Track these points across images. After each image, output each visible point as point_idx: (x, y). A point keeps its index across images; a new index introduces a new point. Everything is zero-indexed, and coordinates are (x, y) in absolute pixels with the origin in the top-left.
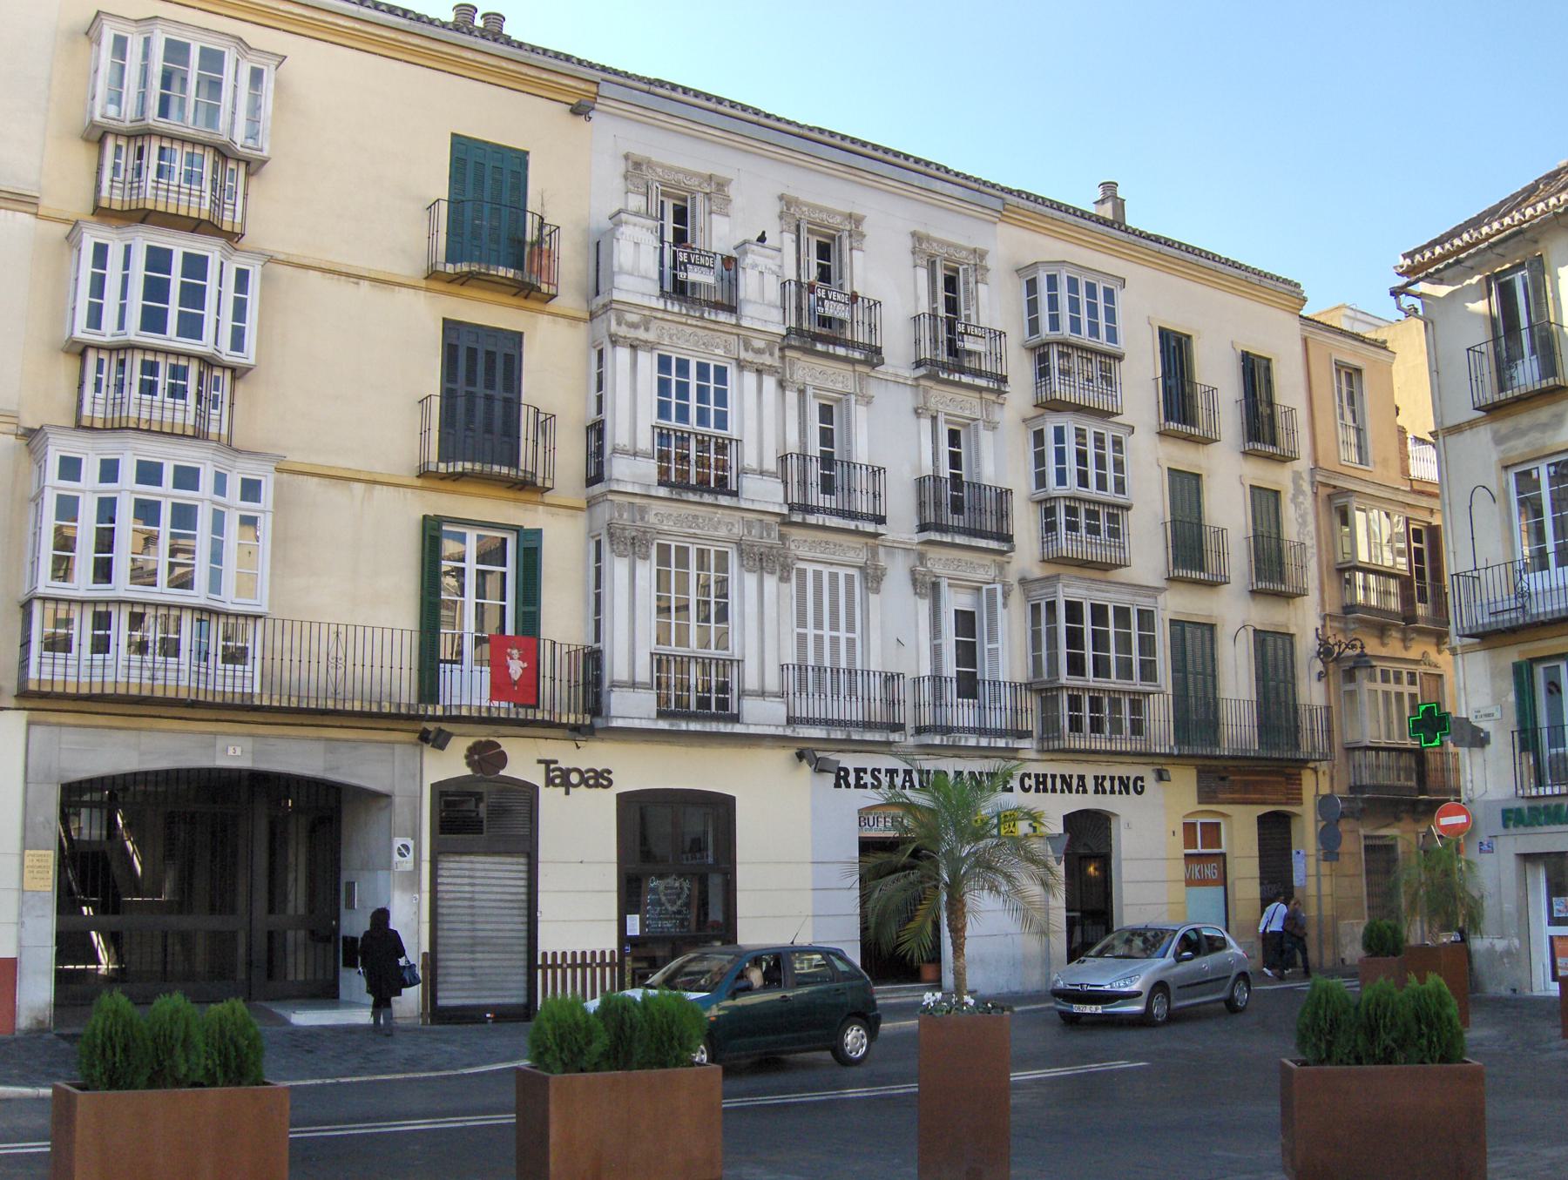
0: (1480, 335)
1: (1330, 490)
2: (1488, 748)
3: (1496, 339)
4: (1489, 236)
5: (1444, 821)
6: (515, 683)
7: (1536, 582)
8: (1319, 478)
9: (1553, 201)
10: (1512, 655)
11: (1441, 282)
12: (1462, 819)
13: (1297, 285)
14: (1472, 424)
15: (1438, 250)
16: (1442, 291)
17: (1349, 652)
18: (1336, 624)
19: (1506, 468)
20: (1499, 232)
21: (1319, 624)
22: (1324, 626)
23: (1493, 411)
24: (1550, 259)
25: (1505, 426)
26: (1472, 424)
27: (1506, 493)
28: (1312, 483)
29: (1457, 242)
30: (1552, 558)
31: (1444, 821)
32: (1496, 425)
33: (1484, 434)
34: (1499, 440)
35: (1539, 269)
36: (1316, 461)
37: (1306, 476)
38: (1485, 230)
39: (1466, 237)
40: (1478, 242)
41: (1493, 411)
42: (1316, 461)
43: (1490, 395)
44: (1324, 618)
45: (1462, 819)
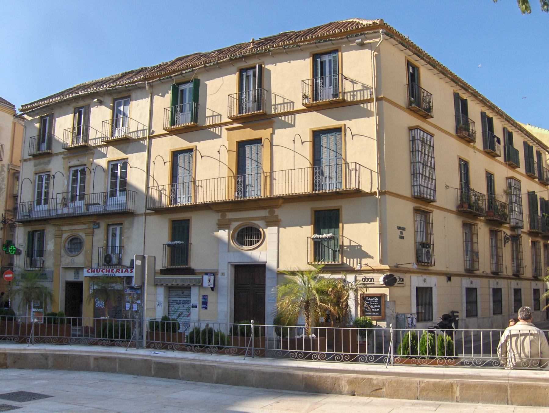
0: (35, 133)
1: (14, 171)
2: (21, 255)
3: (73, 128)
4: (41, 105)
5: (6, 276)
6: (93, 160)
7: (37, 208)
8: (10, 167)
9: (56, 99)
10: (29, 229)
11: (30, 116)
12: (11, 275)
13: (14, 106)
14: (30, 159)
15: (29, 106)
16: (30, 118)
17: (10, 222)
18: (10, 213)
19: (36, 174)
20: (43, 104)
21: (4, 212)
22: (5, 213)
23: (35, 156)
24: (55, 115)
25: (37, 161)
26: (30, 159)
27: (35, 182)
28: (8, 168)
29: (34, 105)
30: (43, 201)
31: (6, 276)
32: (36, 161)
33: (32, 163)
34: (35, 165)
35: (52, 118)
36: (11, 162)
37: (6, 166)
38: (40, 103)
39: (29, 106)
40: (39, 106)
41: (35, 156)
42: (11, 162)
43: (35, 151)
44: (6, 211)
45: (11, 275)
